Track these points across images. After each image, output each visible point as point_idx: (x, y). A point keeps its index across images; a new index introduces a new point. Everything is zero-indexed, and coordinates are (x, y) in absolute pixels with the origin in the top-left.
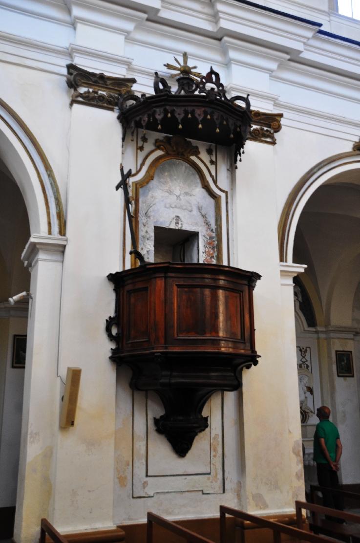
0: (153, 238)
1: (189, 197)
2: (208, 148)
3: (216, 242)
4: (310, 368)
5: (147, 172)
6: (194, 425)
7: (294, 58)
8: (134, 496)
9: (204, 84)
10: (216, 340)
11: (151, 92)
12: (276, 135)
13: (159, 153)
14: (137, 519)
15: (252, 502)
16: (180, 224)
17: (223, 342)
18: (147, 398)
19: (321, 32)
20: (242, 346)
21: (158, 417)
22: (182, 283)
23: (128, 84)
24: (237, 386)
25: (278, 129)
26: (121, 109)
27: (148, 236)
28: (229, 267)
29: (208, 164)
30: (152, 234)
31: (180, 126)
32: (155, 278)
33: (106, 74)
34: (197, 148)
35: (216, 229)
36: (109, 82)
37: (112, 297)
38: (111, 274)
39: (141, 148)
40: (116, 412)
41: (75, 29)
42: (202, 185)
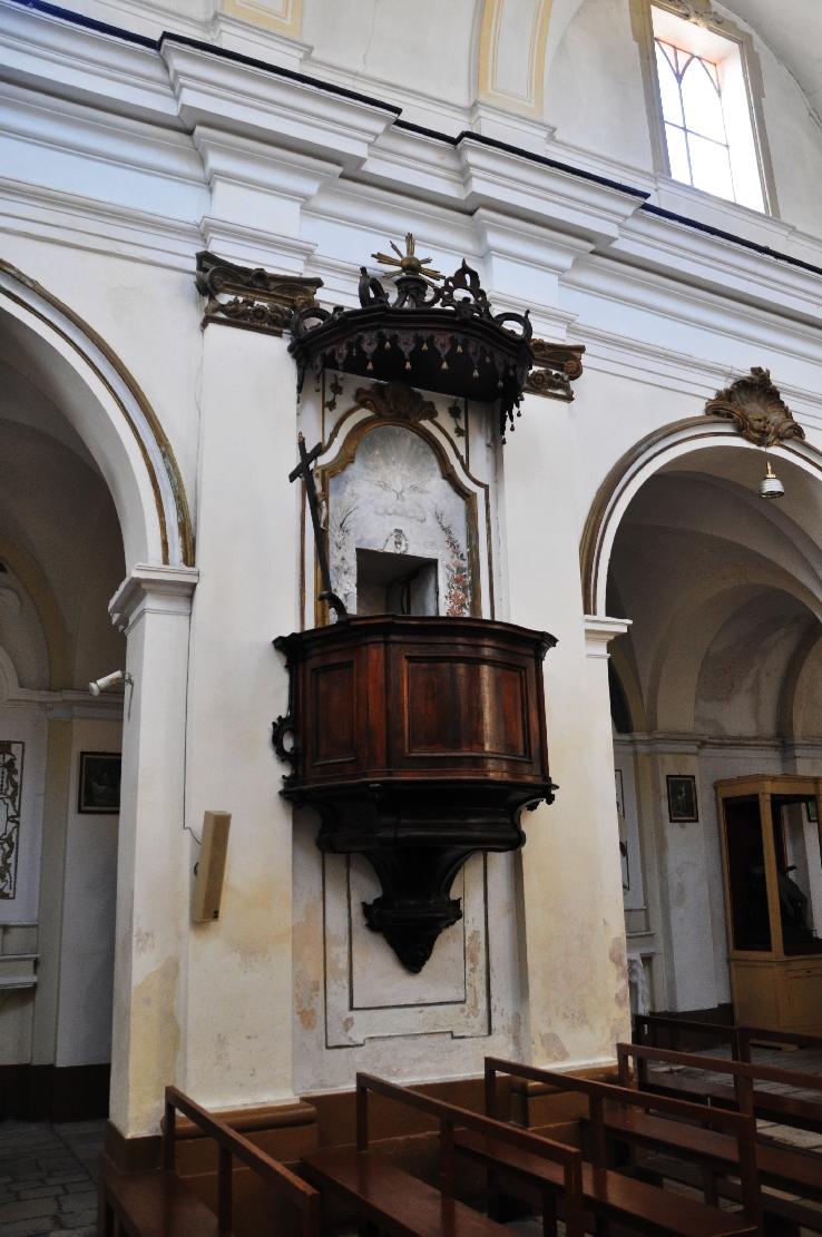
1: (419, 495)
2: (451, 405)
5: (343, 448)
6: (438, 915)
7: (601, 249)
8: (329, 1045)
9: (451, 290)
11: (354, 303)
12: (573, 385)
16: (403, 543)
17: (490, 761)
18: (348, 866)
19: (400, 123)
20: (526, 768)
21: (370, 901)
22: (416, 653)
24: (513, 842)
25: (576, 373)
26: (295, 333)
27: (346, 567)
28: (493, 622)
29: (453, 435)
32: (366, 644)
33: (269, 270)
34: (431, 404)
35: (470, 554)
36: (273, 285)
37: (283, 679)
38: (280, 638)
40: (294, 896)
41: (211, 191)
42: (443, 473)
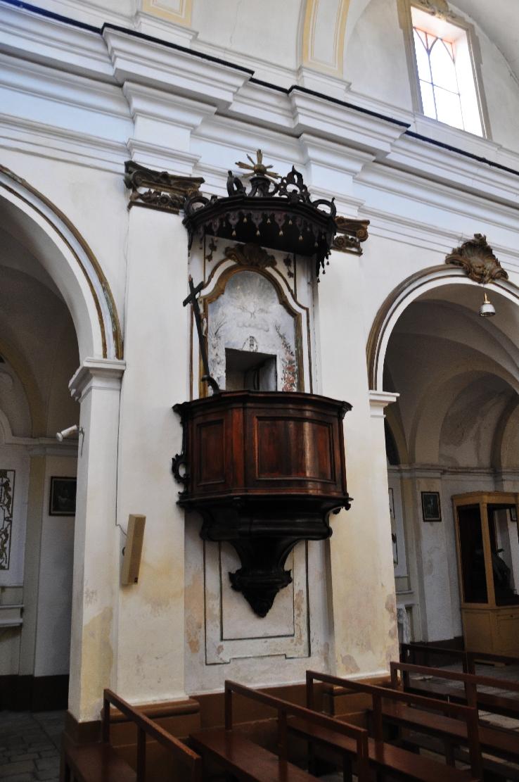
0: (224, 362)
3: (297, 367)
5: (217, 285)
6: (277, 580)
7: (380, 159)
8: (208, 663)
9: (285, 185)
10: (305, 481)
12: (363, 245)
13: (230, 263)
14: (211, 689)
15: (342, 666)
16: (255, 345)
20: (332, 487)
21: (234, 572)
22: (262, 414)
23: (195, 184)
25: (364, 237)
26: (187, 212)
27: (218, 360)
28: (311, 395)
30: (223, 358)
31: (258, 233)
32: (232, 409)
33: (170, 173)
34: (273, 257)
35: (297, 352)
37: (179, 431)
38: (177, 405)
39: (210, 258)
40: (186, 567)
41: (134, 122)
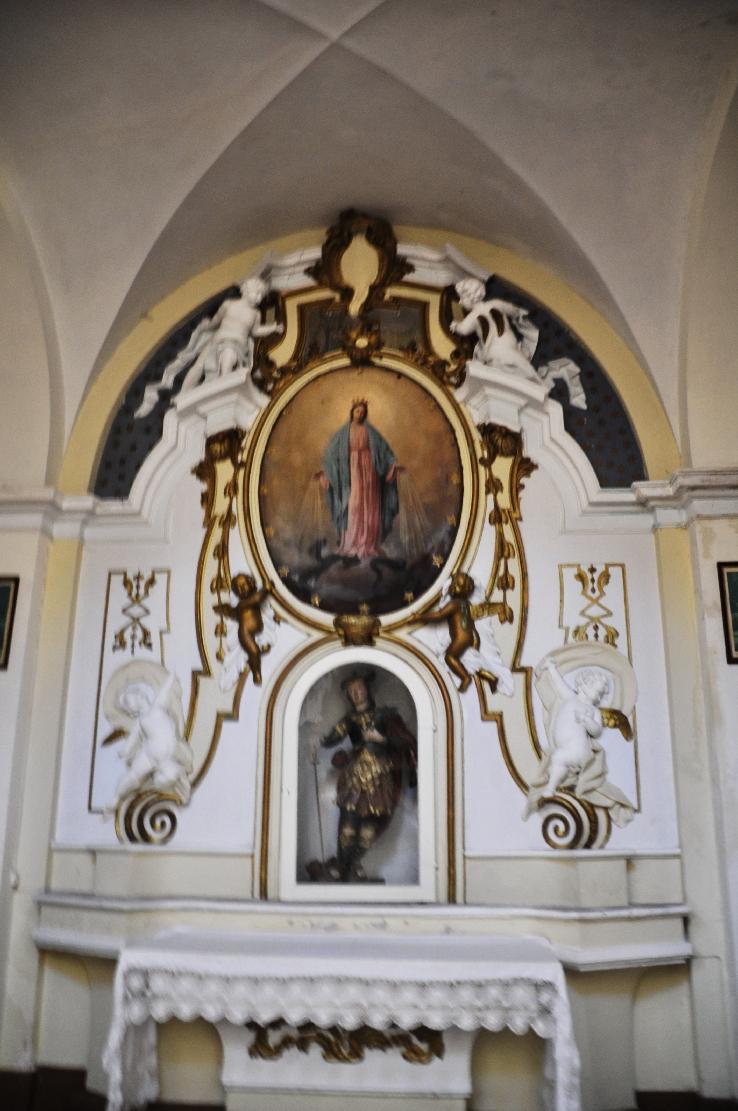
4: (621, 641)
